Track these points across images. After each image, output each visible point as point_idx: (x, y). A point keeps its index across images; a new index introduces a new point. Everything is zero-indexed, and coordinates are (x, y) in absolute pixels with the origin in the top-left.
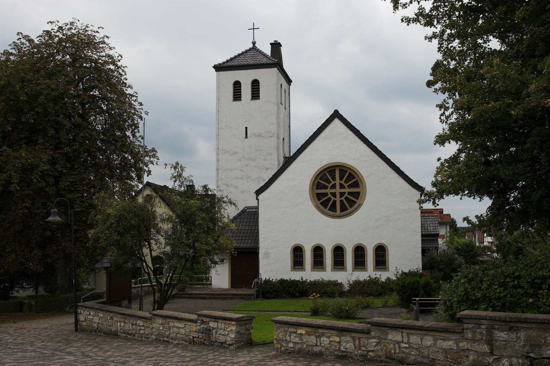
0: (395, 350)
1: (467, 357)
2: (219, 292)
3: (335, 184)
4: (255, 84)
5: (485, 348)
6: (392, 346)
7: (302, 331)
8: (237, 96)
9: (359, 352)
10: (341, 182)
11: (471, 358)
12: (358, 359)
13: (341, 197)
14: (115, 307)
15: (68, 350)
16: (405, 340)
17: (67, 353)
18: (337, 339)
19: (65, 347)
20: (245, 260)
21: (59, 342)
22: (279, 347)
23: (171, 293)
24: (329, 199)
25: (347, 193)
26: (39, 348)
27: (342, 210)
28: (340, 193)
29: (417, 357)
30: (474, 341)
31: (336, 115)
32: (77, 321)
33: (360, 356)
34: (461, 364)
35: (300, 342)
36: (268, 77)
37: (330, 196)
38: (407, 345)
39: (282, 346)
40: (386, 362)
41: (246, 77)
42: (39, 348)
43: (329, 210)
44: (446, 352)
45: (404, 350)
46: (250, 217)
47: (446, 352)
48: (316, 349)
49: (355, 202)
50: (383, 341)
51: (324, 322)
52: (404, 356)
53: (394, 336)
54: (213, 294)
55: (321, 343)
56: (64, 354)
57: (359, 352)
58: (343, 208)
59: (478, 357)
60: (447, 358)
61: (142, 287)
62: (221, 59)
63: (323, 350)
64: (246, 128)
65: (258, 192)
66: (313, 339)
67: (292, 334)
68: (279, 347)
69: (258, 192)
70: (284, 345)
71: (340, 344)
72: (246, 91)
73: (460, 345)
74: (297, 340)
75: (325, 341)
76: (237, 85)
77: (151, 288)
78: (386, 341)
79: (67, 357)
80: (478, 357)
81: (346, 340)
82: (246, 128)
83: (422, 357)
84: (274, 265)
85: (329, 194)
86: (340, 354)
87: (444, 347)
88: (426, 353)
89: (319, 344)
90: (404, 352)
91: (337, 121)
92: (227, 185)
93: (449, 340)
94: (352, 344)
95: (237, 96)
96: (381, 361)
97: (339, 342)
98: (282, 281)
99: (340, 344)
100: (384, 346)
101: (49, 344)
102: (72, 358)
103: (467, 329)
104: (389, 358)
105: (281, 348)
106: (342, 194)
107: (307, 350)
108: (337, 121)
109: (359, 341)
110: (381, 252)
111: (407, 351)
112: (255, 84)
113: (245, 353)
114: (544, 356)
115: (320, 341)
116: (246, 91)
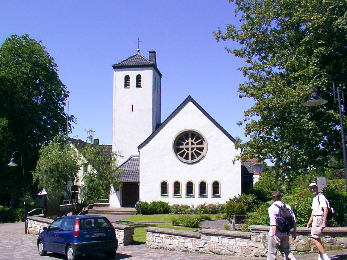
0: (214, 247)
1: (253, 251)
2: (114, 210)
3: (185, 148)
4: (139, 78)
5: (262, 246)
6: (213, 245)
7: (163, 236)
8: (127, 85)
9: (195, 248)
10: (188, 152)
11: (255, 251)
12: (194, 252)
13: (192, 151)
14: (49, 219)
15: (23, 246)
16: (220, 242)
17: (23, 247)
18: (183, 241)
19: (21, 244)
20: (130, 192)
21: (16, 240)
22: (149, 245)
23: (84, 210)
24: (185, 152)
25: (195, 148)
26: (5, 244)
27: (192, 159)
28: (191, 145)
29: (226, 251)
30: (257, 242)
31: (189, 99)
32: (26, 227)
33: (195, 250)
34: (249, 254)
35: (161, 242)
36: (147, 75)
37: (185, 150)
38: (221, 244)
39: (151, 244)
40: (209, 254)
41: (133, 74)
42: (5, 244)
43: (184, 159)
44: (242, 248)
45: (219, 247)
46: (133, 161)
47: (242, 248)
48: (171, 247)
49: (200, 154)
50: (208, 242)
51: (175, 231)
52: (219, 250)
53: (214, 239)
54: (110, 211)
55: (173, 243)
56: (20, 248)
57: (195, 248)
58: (193, 158)
59: (258, 251)
60: (242, 251)
61: (66, 206)
62: (117, 62)
63: (175, 247)
64: (133, 105)
65: (140, 147)
66: (169, 241)
67: (157, 237)
68: (149, 245)
69: (140, 147)
70: (153, 244)
71: (184, 244)
72: (133, 81)
73: (249, 244)
74: (160, 241)
75: (176, 242)
76: (127, 78)
77: (72, 207)
78: (210, 242)
79: (23, 250)
80: (258, 251)
81: (187, 241)
82: (133, 105)
83: (229, 251)
84: (148, 194)
85: (184, 148)
86: (184, 249)
87: (241, 245)
88: (231, 249)
89: (172, 243)
90: (219, 248)
91: (190, 104)
92: (120, 142)
93: (244, 241)
94: (191, 244)
95: (127, 85)
96: (207, 253)
97: (184, 243)
98: (154, 203)
99: (184, 244)
100: (209, 245)
101: (10, 242)
102: (26, 251)
103: (253, 235)
104: (211, 252)
105: (150, 245)
106: (192, 149)
107: (165, 247)
108: (190, 104)
109: (195, 242)
110: (216, 186)
111: (221, 247)
112: (139, 78)
113: (130, 248)
114: (292, 249)
115: (173, 242)
116: (133, 81)
